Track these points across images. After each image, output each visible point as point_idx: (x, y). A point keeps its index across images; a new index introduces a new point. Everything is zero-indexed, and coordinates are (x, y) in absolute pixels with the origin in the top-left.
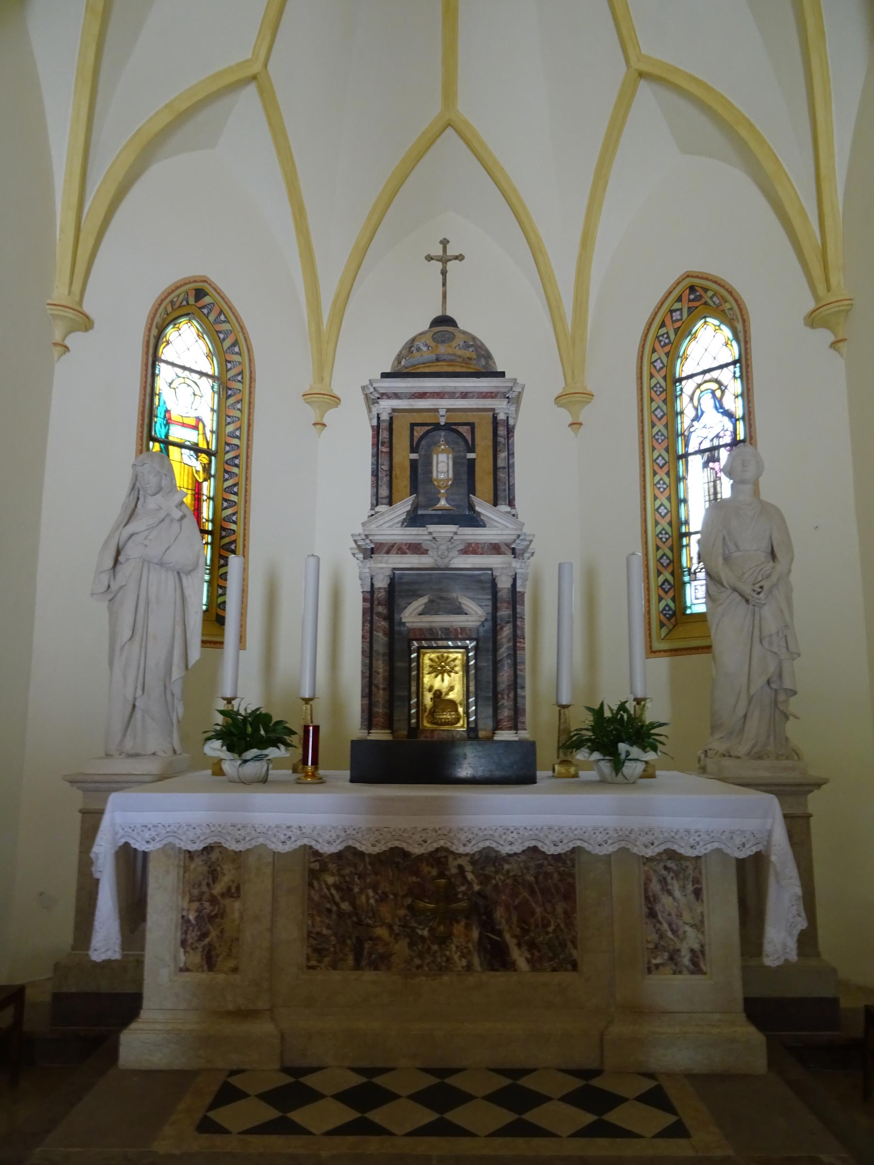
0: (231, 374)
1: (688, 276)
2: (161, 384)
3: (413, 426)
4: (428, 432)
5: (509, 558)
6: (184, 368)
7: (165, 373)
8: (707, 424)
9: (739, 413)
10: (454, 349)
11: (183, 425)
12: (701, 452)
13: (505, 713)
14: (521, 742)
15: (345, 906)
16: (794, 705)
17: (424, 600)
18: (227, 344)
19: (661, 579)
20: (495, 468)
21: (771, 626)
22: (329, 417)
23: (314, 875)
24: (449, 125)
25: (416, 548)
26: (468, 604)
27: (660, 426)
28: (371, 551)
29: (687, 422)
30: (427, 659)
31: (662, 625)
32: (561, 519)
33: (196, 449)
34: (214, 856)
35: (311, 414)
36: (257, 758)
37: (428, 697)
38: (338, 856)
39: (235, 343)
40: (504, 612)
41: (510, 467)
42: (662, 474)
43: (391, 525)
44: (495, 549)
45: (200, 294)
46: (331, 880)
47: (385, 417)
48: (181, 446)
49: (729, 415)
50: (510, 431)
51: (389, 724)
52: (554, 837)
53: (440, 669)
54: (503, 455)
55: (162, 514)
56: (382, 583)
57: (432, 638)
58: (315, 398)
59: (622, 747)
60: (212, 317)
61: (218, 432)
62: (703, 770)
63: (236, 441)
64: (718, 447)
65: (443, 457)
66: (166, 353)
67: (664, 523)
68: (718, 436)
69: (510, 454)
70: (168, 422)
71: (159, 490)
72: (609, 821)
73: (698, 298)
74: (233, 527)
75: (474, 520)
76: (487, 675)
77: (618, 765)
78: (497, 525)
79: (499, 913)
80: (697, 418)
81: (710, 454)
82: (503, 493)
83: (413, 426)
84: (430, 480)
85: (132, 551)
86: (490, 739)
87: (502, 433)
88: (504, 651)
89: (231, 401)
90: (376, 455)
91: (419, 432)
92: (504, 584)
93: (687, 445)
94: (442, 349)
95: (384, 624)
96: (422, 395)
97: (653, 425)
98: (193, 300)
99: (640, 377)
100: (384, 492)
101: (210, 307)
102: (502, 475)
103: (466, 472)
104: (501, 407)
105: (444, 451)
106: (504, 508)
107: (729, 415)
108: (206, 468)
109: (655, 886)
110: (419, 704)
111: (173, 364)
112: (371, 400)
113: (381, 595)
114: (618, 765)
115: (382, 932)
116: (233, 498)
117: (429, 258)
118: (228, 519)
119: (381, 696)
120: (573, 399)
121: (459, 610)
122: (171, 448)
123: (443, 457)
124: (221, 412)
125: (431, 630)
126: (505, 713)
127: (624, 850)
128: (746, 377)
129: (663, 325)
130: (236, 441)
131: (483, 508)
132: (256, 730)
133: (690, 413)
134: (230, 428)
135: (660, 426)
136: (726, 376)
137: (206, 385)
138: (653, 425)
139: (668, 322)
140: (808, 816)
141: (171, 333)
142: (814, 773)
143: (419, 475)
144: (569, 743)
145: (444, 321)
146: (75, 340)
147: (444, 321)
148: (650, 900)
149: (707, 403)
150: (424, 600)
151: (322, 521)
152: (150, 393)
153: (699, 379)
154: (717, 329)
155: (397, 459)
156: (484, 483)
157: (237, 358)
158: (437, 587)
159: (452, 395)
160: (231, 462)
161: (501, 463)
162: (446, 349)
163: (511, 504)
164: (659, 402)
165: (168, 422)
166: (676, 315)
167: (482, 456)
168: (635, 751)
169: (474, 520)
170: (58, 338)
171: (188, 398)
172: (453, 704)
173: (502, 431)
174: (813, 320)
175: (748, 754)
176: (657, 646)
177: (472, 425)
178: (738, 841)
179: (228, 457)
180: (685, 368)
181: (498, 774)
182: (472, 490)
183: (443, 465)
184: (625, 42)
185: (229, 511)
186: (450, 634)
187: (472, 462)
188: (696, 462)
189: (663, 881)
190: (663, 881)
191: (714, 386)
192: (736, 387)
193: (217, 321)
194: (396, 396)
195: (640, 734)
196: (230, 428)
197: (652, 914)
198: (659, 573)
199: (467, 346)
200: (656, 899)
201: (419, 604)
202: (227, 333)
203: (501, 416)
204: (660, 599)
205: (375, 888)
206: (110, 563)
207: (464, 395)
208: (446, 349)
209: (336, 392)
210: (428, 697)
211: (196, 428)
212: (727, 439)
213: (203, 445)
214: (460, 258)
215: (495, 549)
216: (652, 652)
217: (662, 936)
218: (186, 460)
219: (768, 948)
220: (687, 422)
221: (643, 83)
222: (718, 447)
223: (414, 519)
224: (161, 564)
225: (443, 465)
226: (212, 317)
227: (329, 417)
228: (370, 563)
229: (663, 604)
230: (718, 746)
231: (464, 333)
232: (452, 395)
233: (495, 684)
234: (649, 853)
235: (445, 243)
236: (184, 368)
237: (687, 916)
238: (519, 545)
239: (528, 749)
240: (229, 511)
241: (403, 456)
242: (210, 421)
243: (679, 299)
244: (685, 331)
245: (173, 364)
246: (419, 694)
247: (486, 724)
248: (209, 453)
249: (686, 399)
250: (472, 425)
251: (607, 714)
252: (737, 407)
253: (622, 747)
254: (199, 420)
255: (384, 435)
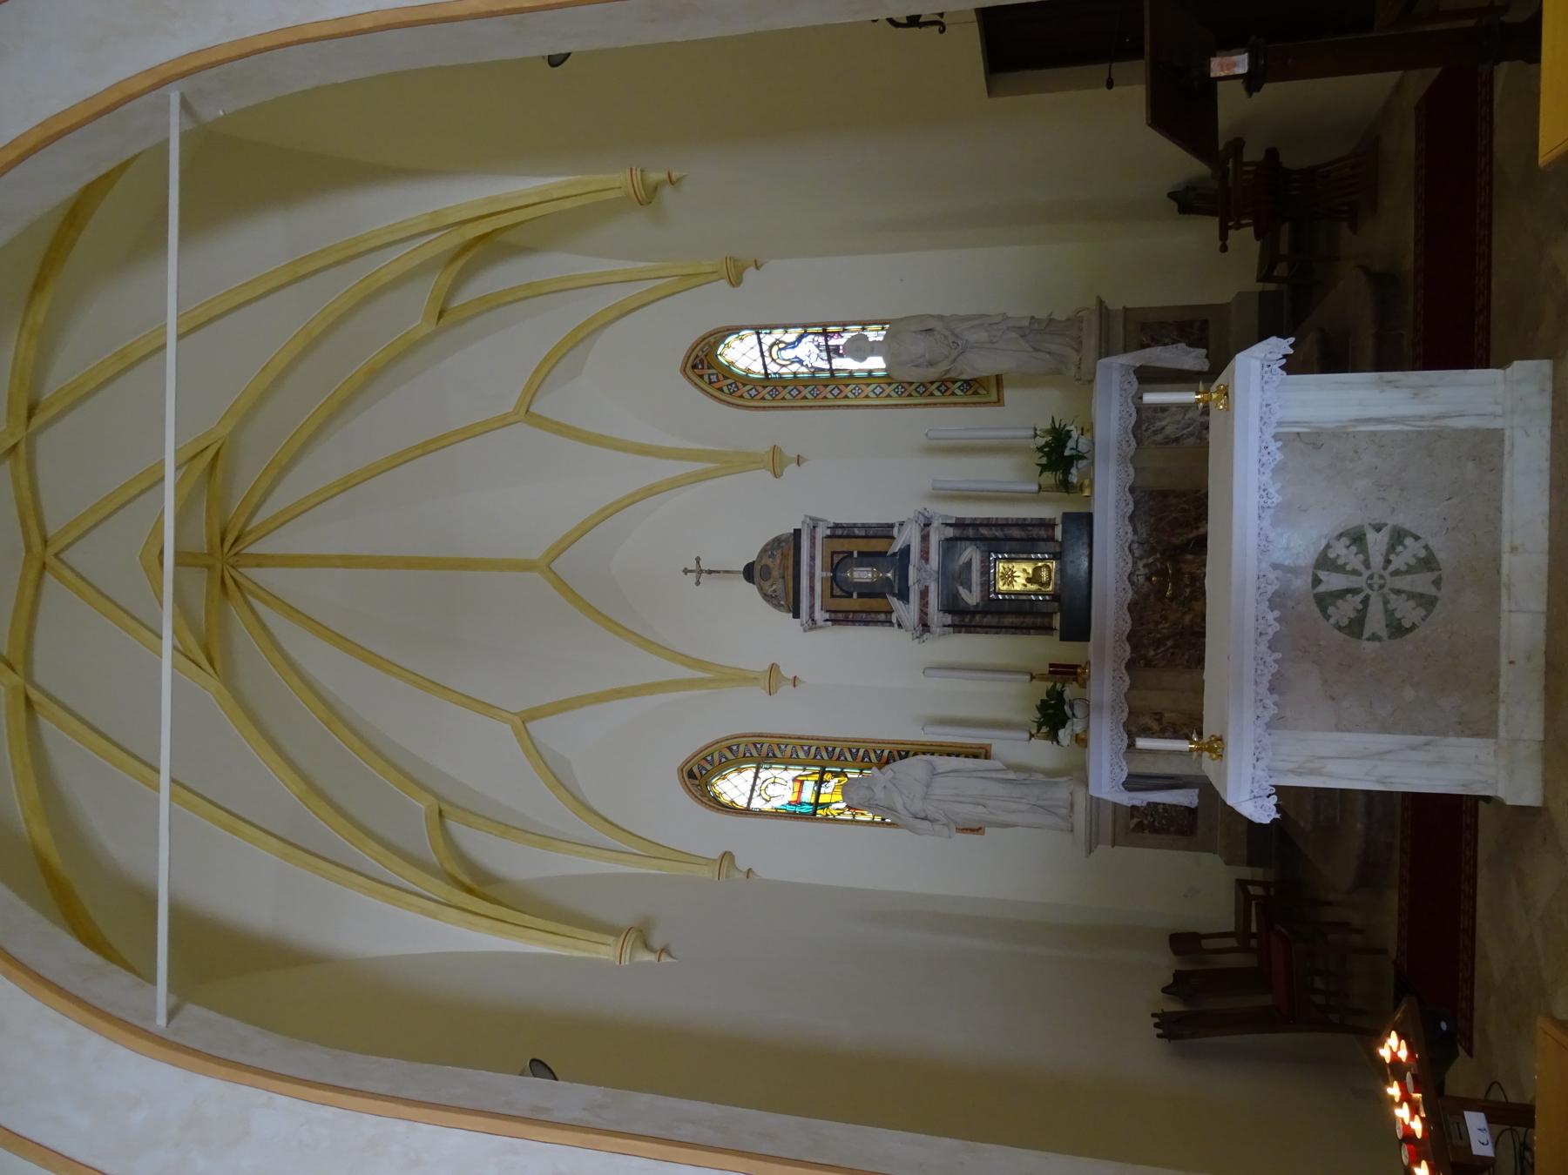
0: (755, 753)
1: (684, 370)
2: (767, 807)
3: (832, 596)
4: (838, 586)
5: (932, 529)
6: (753, 790)
7: (757, 804)
8: (809, 354)
9: (800, 330)
10: (775, 565)
11: (800, 792)
12: (829, 360)
13: (1043, 533)
14: (1063, 523)
15: (1170, 643)
16: (1042, 315)
17: (961, 589)
18: (730, 756)
19: (937, 393)
20: (866, 537)
21: (983, 336)
22: (788, 673)
23: (1149, 664)
24: (548, 566)
25: (924, 594)
26: (964, 558)
27: (805, 392)
28: (925, 626)
29: (804, 370)
30: (1002, 586)
31: (975, 393)
32: (894, 478)
33: (820, 783)
34: (1134, 729)
35: (786, 688)
36: (1072, 707)
37: (1033, 587)
38: (1134, 649)
39: (730, 748)
40: (971, 532)
41: (864, 526)
42: (847, 391)
43: (907, 612)
44: (925, 538)
45: (691, 775)
46: (1152, 653)
47: (827, 616)
48: (818, 794)
49: (800, 339)
50: (837, 526)
51: (1050, 615)
52: (1123, 504)
53: (1010, 578)
54: (857, 531)
55: (889, 785)
56: (948, 619)
57: (988, 583)
58: (773, 683)
59: (1067, 453)
60: (709, 767)
61: (805, 766)
62: (1091, 382)
63: (813, 750)
64: (827, 346)
65: (856, 575)
66: (742, 802)
67: (889, 390)
68: (818, 346)
69: (854, 526)
70: (799, 803)
71: (869, 788)
72: (1113, 468)
73: (703, 364)
74: (886, 753)
75: (906, 551)
76: (1014, 545)
77: (1081, 457)
78: (909, 537)
79: (1176, 541)
80: (801, 362)
81: (832, 352)
82: (885, 532)
83: (832, 596)
84: (873, 584)
85: (918, 806)
86: (1061, 544)
87: (840, 532)
88: (998, 534)
89: (778, 753)
90: (853, 622)
91: (837, 591)
92: (950, 532)
93: (823, 370)
94: (776, 573)
95: (978, 618)
96: (812, 589)
97: (805, 398)
98: (698, 776)
99: (764, 408)
100: (882, 617)
101: (701, 768)
102: (871, 533)
103: (867, 558)
104: (822, 532)
105: (848, 576)
106: (895, 531)
107: (800, 339)
108: (836, 775)
109: (1159, 438)
110: (1036, 594)
111: (750, 799)
112: (813, 624)
113: (957, 619)
114: (1081, 457)
115: (1188, 618)
116: (861, 752)
117: (698, 583)
118: (879, 757)
119: (1029, 620)
120: (776, 462)
121: (969, 564)
122: (821, 800)
123: (856, 575)
124: (787, 763)
125: (982, 585)
126: (1043, 533)
127: (1132, 460)
128: (772, 328)
129: (721, 390)
130: (813, 750)
131: (896, 547)
132: (1052, 707)
133: (795, 367)
134: (802, 755)
135: (805, 392)
136: (767, 340)
137: (764, 774)
138: (805, 398)
139: (718, 385)
140: (1125, 309)
141: (725, 799)
142: (1093, 304)
143: (867, 591)
144: (1065, 486)
145: (749, 573)
146: (742, 864)
147: (749, 573)
148: (1168, 441)
149: (789, 354)
150: (961, 589)
151: (885, 675)
152: (776, 814)
153: (768, 360)
154: (728, 346)
155: (856, 608)
156: (877, 545)
157: (742, 748)
158: (952, 578)
159: (812, 567)
160: (831, 754)
161: (863, 533)
162: (776, 572)
163: (891, 526)
164: (784, 393)
165: (799, 803)
166: (714, 378)
167: (856, 547)
168: (1071, 444)
169: (906, 551)
170: (742, 876)
171: (780, 787)
172: (1037, 570)
173: (839, 532)
174: (736, 282)
175: (1078, 351)
176: (994, 397)
177: (833, 553)
178: (1126, 386)
179: (824, 757)
180: (757, 368)
181: (1086, 539)
182: (883, 554)
183: (863, 575)
184: (503, 422)
185: (873, 756)
186: (985, 571)
187: (860, 553)
188: (838, 363)
189: (1155, 432)
190: (1155, 432)
191: (775, 349)
192: (778, 334)
193: (711, 763)
194: (812, 607)
195: (1059, 436)
196: (802, 755)
197: (1177, 440)
198: (932, 394)
199: (772, 556)
200: (1167, 437)
201: (963, 592)
202: (722, 755)
203: (828, 532)
204: (954, 394)
205: (1158, 623)
206: (926, 824)
207: (813, 558)
208: (776, 572)
209: (767, 667)
210: (1033, 587)
211: (802, 782)
212: (821, 340)
213: (816, 777)
214: (698, 560)
215: (925, 538)
216: (999, 401)
217: (1191, 434)
218: (830, 790)
219: (1197, 368)
220: (804, 370)
221: (539, 408)
222: (827, 346)
223: (904, 596)
224: (928, 786)
225: (863, 575)
226: (709, 767)
227: (788, 673)
228: (934, 628)
229: (958, 392)
230: (1073, 371)
231: (760, 556)
232: (812, 567)
233: (1022, 540)
234: (1134, 444)
235: (686, 571)
236: (753, 790)
237: (1179, 417)
238: (922, 521)
239: (1067, 517)
240: (873, 756)
241: (855, 603)
242: (794, 772)
243: (701, 377)
244: (727, 371)
245: (750, 799)
246: (1028, 593)
247: (1051, 547)
248: (823, 773)
249: (784, 370)
250: (833, 553)
251: (1044, 461)
252: (791, 336)
253: (1067, 453)
254: (795, 780)
255: (840, 616)
